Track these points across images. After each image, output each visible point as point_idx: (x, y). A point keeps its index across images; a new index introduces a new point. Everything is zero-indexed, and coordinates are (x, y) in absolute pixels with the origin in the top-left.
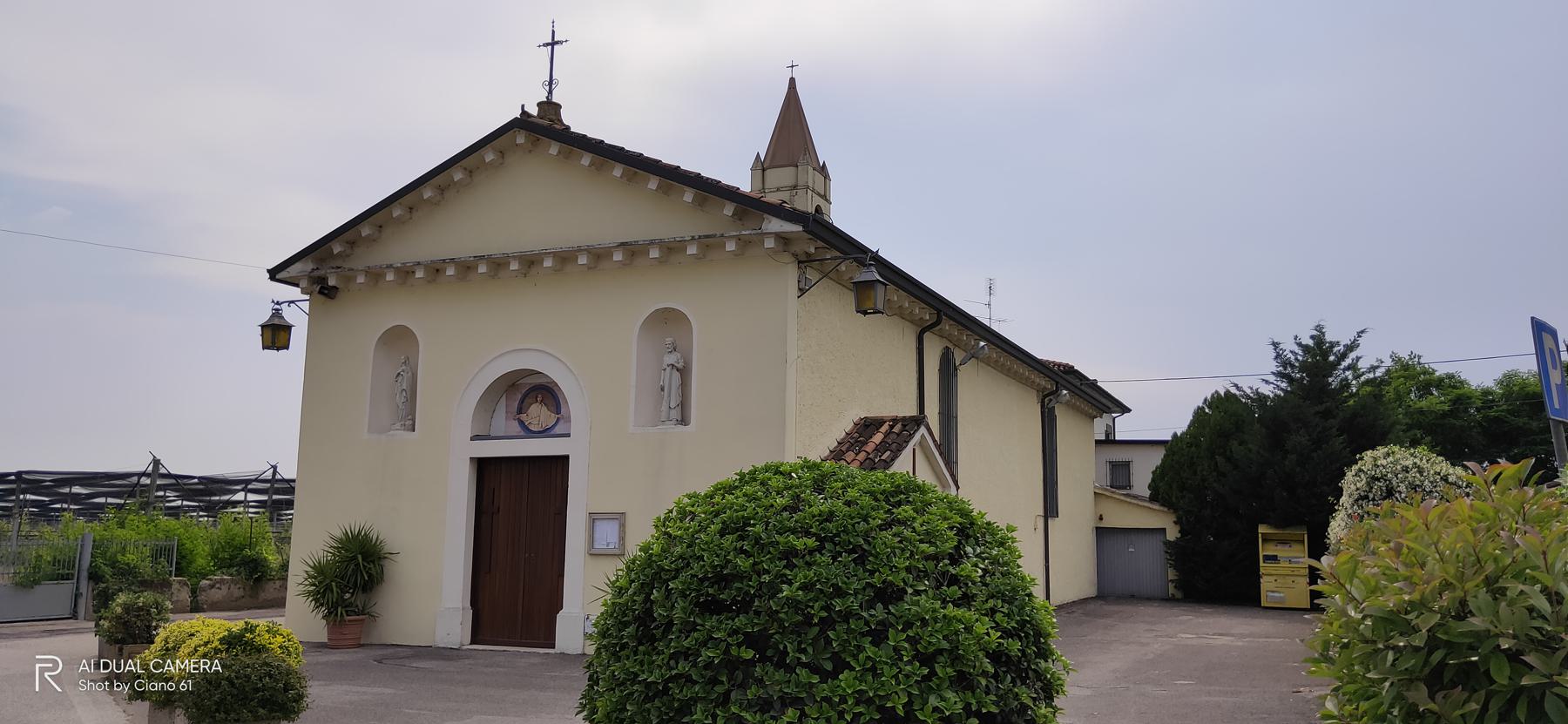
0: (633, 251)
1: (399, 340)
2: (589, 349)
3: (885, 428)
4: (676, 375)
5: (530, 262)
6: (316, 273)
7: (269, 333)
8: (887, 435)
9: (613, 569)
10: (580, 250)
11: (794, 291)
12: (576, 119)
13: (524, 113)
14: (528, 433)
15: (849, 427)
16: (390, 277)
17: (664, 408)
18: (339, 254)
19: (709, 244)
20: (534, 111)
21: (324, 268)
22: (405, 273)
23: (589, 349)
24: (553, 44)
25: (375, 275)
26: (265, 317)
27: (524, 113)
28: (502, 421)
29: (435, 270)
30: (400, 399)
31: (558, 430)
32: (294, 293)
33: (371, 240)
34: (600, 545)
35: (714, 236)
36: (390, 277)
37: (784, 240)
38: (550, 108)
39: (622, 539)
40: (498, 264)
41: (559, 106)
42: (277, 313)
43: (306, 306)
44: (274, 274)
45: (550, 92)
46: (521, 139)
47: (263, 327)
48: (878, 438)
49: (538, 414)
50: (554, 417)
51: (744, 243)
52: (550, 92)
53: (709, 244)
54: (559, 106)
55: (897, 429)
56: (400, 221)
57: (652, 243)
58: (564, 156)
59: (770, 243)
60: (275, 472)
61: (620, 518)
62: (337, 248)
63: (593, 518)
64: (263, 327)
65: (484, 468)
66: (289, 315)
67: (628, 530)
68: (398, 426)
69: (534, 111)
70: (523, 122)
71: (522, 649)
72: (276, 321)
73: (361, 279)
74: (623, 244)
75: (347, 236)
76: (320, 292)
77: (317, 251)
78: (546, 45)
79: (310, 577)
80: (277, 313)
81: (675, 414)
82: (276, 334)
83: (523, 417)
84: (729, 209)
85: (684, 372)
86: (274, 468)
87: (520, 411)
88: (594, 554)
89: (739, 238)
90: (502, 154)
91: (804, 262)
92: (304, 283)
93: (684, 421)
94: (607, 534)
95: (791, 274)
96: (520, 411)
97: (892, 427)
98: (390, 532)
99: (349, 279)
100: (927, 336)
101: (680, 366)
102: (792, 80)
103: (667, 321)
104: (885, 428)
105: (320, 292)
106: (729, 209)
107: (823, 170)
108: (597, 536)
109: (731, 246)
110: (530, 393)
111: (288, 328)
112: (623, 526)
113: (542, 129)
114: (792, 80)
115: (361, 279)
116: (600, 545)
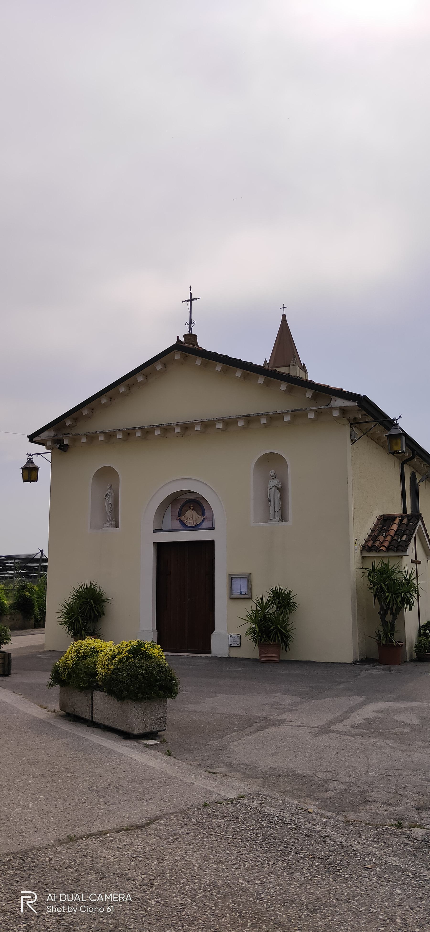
0: (250, 419)
1: (107, 474)
2: (225, 478)
3: (397, 521)
4: (278, 492)
5: (186, 428)
6: (57, 437)
7: (27, 473)
8: (400, 525)
9: (248, 608)
10: (218, 420)
11: (349, 442)
12: (203, 343)
13: (179, 341)
14: (186, 528)
15: (375, 521)
16: (101, 438)
17: (271, 512)
18: (69, 426)
19: (297, 415)
20: (182, 339)
21: (61, 435)
22: (110, 436)
23: (225, 478)
24: (191, 300)
25: (92, 438)
26: (24, 462)
27: (179, 341)
28: (169, 521)
29: (128, 433)
30: (108, 509)
31: (204, 525)
32: (42, 449)
33: (88, 417)
34: (236, 593)
35: (301, 410)
36: (101, 438)
37: (343, 411)
38: (191, 337)
39: (250, 589)
40: (167, 430)
41: (196, 336)
42: (30, 460)
43: (49, 456)
44: (32, 438)
45: (190, 328)
46: (178, 357)
47: (23, 469)
48: (395, 527)
49: (191, 517)
50: (200, 519)
51: (318, 413)
52: (190, 328)
53: (297, 415)
54: (196, 336)
55: (405, 521)
56: (105, 406)
57: (262, 415)
58: (204, 365)
59: (336, 413)
60: (42, 554)
61: (248, 577)
62: (68, 423)
63: (232, 577)
64: (23, 469)
65: (161, 548)
66: (37, 461)
67: (253, 584)
68: (108, 524)
69: (182, 339)
70: (178, 346)
71: (191, 655)
72: (31, 465)
73: (84, 440)
74: (244, 416)
75: (74, 415)
76: (59, 448)
77: (57, 424)
78: (193, 300)
79: (65, 613)
80: (30, 460)
81: (278, 515)
82: (30, 473)
83: (182, 518)
84: (309, 394)
85: (282, 490)
86: (42, 551)
87: (180, 514)
88: (232, 598)
89: (316, 411)
90: (165, 365)
91: (354, 423)
92: (49, 443)
93: (283, 518)
94: (241, 586)
95: (347, 430)
96: (180, 514)
97: (401, 521)
98: (107, 587)
99: (76, 439)
100: (405, 465)
101: (279, 486)
102: (284, 316)
103: (271, 462)
104: (397, 521)
105: (59, 448)
106: (309, 394)
107: (303, 367)
108: (234, 587)
109: (311, 416)
110: (187, 505)
111: (36, 469)
112: (250, 582)
113: (187, 349)
114: (284, 316)
115: (84, 440)
116: (236, 593)
